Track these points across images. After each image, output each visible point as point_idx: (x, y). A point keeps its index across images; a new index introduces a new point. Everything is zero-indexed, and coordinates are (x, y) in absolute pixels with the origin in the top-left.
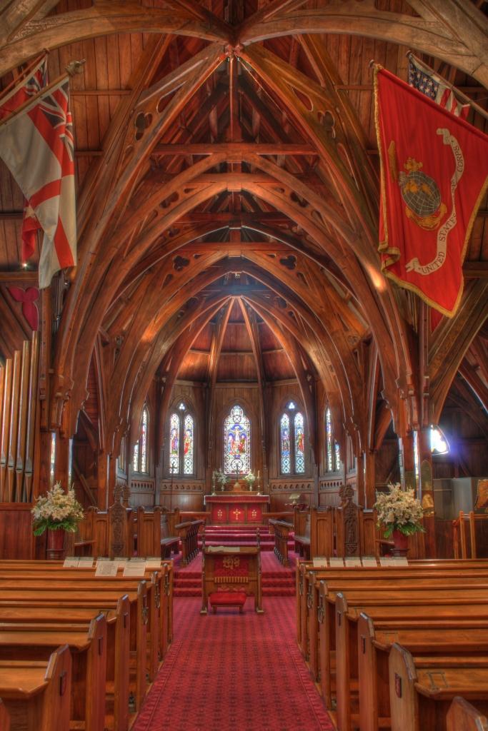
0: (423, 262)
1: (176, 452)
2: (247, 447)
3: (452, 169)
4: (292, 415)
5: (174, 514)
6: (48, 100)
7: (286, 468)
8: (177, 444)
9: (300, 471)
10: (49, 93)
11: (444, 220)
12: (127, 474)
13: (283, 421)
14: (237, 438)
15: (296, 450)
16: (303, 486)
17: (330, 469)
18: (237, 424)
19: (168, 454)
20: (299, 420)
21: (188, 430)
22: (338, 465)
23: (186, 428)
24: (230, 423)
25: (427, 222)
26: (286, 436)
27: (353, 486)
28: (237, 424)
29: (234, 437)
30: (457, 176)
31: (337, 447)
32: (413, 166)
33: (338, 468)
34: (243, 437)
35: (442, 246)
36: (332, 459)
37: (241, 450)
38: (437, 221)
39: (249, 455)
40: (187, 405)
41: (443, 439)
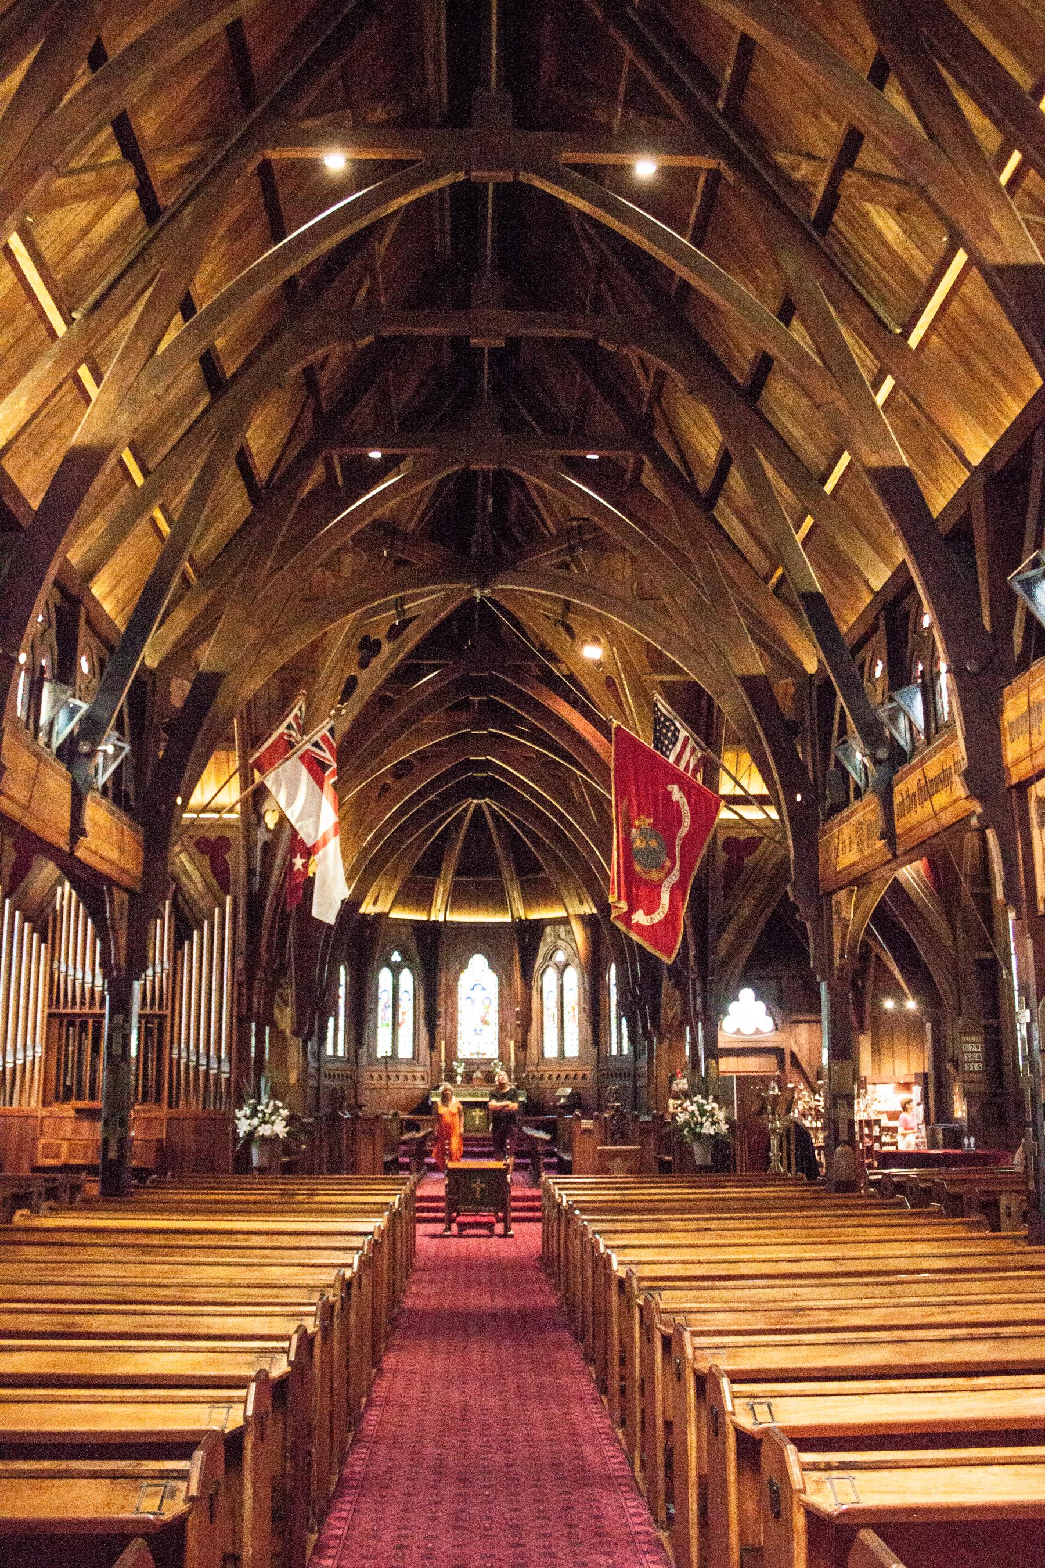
0: (649, 912)
4: (561, 970)
5: (391, 1120)
6: (316, 745)
7: (551, 1051)
11: (667, 875)
12: (319, 1059)
16: (575, 1077)
25: (654, 876)
27: (188, 1463)
28: (477, 984)
34: (487, 1001)
35: (665, 898)
38: (662, 875)
40: (402, 953)
41: (725, 1013)
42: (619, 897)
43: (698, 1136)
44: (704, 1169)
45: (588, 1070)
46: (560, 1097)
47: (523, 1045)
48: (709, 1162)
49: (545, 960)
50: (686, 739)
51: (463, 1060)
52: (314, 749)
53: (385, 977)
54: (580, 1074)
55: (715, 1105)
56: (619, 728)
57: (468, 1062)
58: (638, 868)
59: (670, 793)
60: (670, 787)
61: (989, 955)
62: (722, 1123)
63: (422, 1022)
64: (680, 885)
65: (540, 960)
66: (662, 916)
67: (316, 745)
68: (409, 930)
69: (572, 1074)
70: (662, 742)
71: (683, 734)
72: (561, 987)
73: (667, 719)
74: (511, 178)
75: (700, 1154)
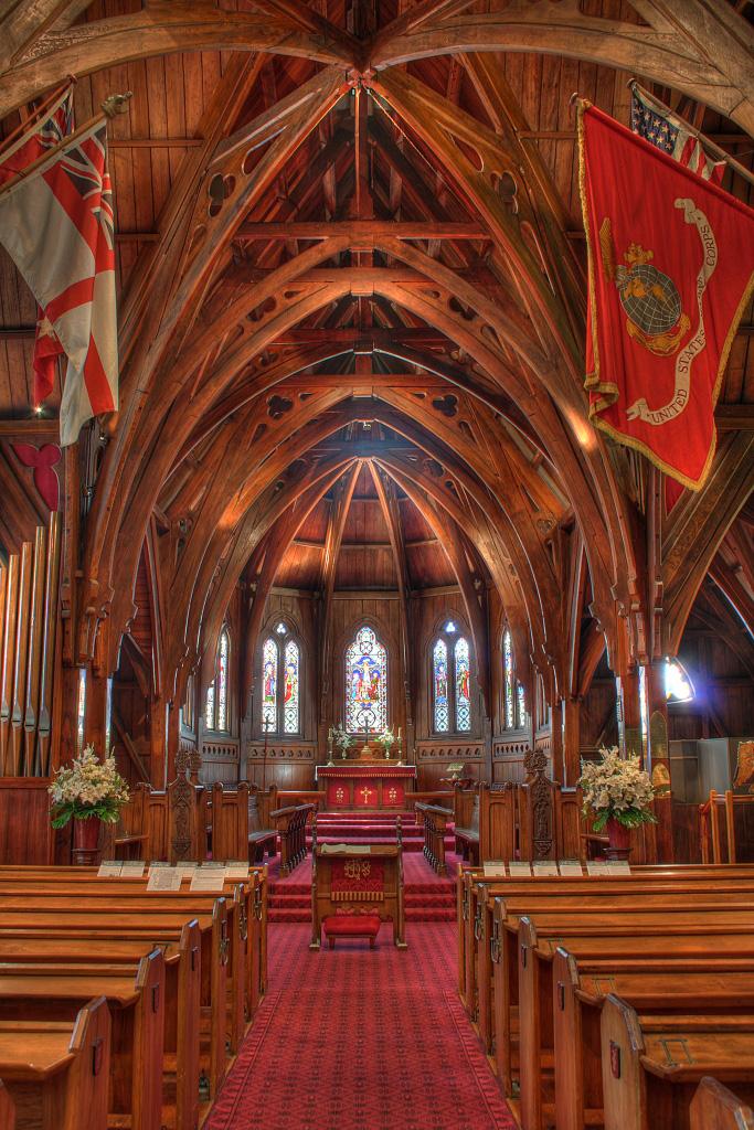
0: (653, 406)
1: (272, 699)
2: (382, 691)
3: (699, 262)
4: (451, 641)
6: (74, 155)
7: (442, 724)
8: (274, 686)
9: (464, 729)
10: (76, 144)
11: (685, 342)
12: (196, 732)
13: (437, 650)
14: (366, 677)
15: (458, 696)
17: (510, 725)
18: (366, 655)
19: (260, 701)
20: (463, 649)
21: (291, 665)
22: (522, 718)
24: (355, 654)
25: (660, 343)
26: (441, 674)
28: (367, 656)
29: (361, 676)
30: (707, 272)
31: (521, 691)
32: (638, 256)
33: (522, 723)
34: (375, 675)
35: (683, 381)
36: (513, 710)
37: (373, 696)
38: (676, 341)
39: (385, 703)
40: (289, 627)
46: (452, 773)
52: (72, 163)
53: (440, 650)
67: (74, 155)
74: (353, 71)
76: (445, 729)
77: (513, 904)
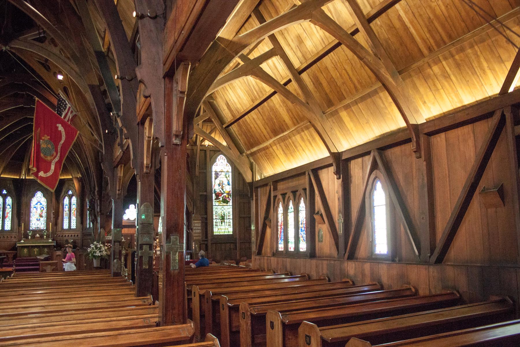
0: (45, 172)
2: (44, 214)
4: (70, 197)
7: (66, 226)
11: (54, 158)
13: (65, 200)
16: (74, 236)
23: (7, 204)
25: (49, 158)
28: (39, 202)
29: (37, 209)
30: (62, 142)
35: (53, 167)
37: (41, 216)
38: (52, 158)
42: (33, 166)
43: (95, 257)
44: (97, 268)
45: (79, 233)
47: (56, 224)
48: (99, 266)
49: (64, 194)
50: (70, 108)
51: (32, 230)
53: (66, 201)
54: (76, 235)
55: (102, 245)
56: (38, 101)
57: (33, 231)
58: (42, 155)
59: (57, 127)
60: (58, 125)
61: (205, 193)
62: (104, 252)
63: (15, 216)
64: (60, 162)
65: (63, 194)
66: (51, 173)
68: (11, 182)
69: (73, 235)
70: (60, 108)
71: (69, 105)
72: (70, 203)
73: (63, 100)
75: (96, 263)
76: (67, 228)
77: (110, 277)
